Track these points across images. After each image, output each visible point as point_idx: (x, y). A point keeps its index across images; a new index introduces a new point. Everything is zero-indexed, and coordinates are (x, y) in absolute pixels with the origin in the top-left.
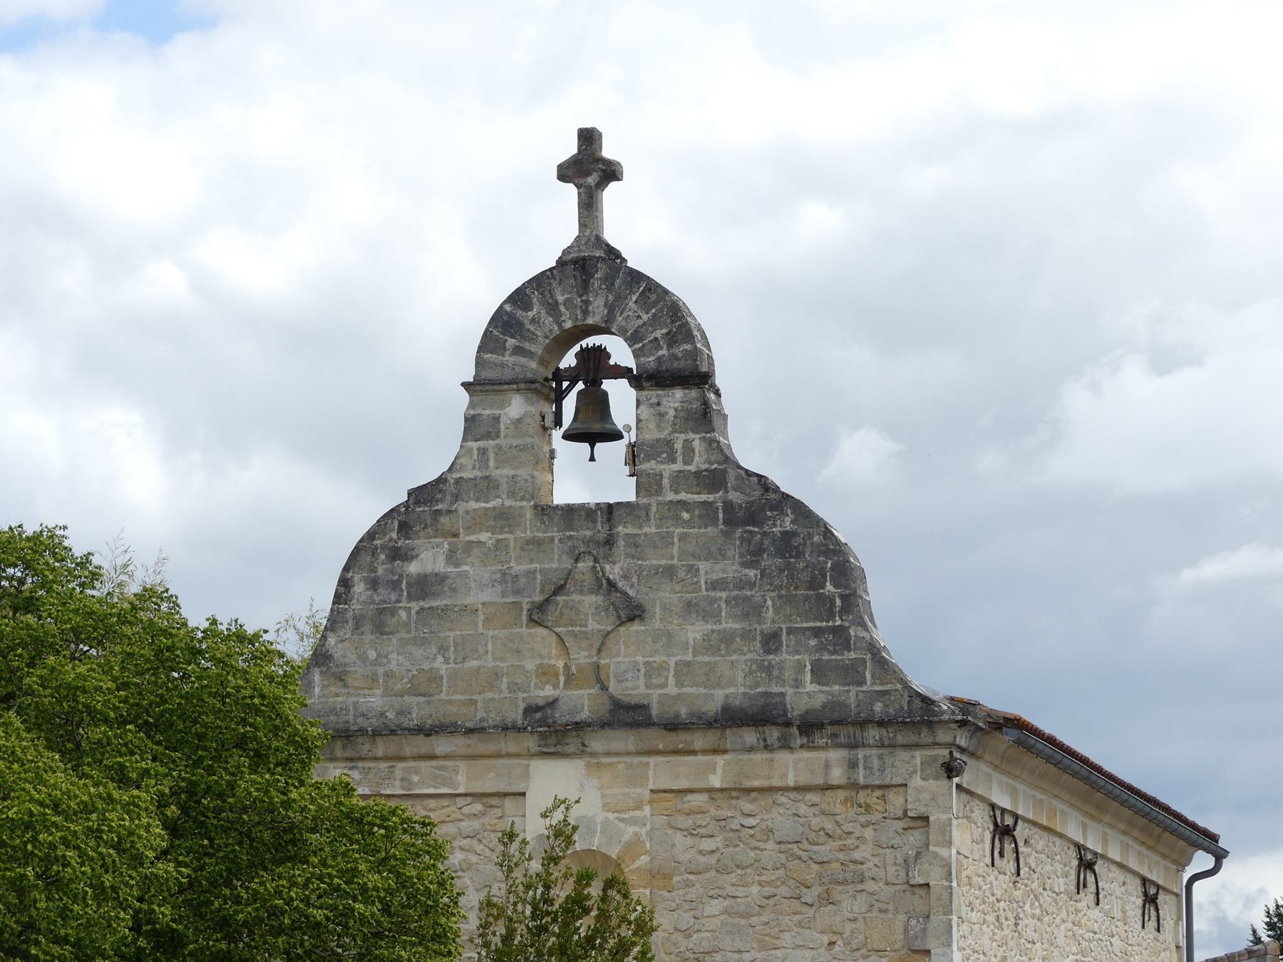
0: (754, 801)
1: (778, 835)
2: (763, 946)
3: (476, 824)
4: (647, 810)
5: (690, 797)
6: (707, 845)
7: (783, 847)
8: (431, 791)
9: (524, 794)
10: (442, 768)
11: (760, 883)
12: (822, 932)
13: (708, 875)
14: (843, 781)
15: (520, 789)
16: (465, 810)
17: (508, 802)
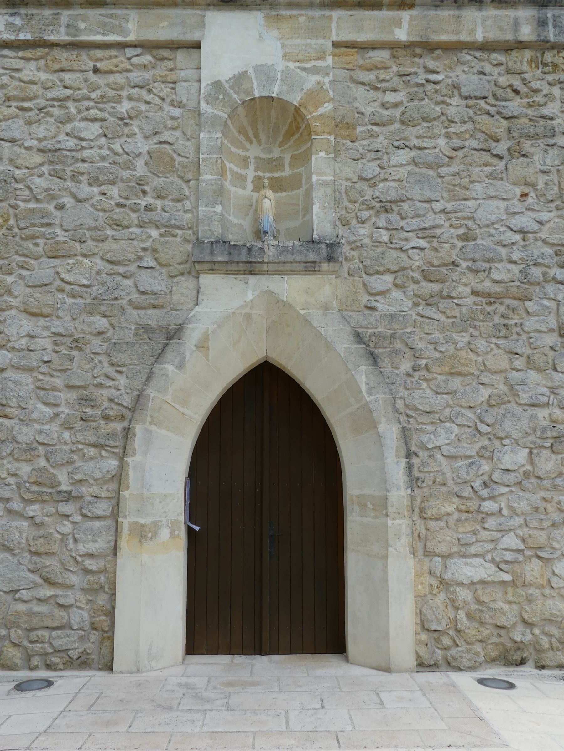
0: (438, 58)
1: (465, 91)
2: (453, 198)
3: (147, 75)
4: (330, 61)
5: (371, 54)
6: (390, 97)
7: (471, 102)
8: (99, 38)
9: (197, 46)
10: (111, 16)
11: (448, 136)
12: (514, 184)
13: (392, 128)
14: (533, 38)
15: (195, 36)
16: (135, 60)
17: (181, 56)
